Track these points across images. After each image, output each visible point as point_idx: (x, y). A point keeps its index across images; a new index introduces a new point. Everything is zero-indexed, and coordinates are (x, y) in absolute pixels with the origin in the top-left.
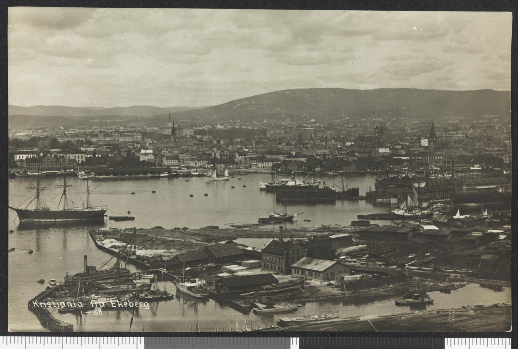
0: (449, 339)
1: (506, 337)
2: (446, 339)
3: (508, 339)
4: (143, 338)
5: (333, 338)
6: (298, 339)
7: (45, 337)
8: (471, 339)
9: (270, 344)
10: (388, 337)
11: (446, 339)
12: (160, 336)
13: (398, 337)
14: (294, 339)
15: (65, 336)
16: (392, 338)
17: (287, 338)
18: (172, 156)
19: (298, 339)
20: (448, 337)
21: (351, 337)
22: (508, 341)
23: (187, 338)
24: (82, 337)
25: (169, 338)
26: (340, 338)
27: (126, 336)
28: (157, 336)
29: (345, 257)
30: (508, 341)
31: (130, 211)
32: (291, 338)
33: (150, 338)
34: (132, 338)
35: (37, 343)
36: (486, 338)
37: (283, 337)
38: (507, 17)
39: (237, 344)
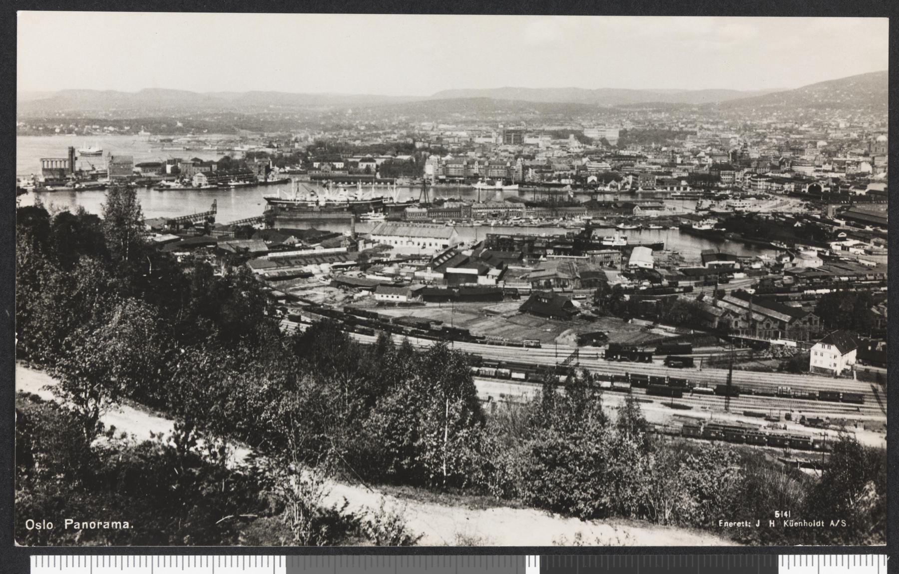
0: (786, 556)
1: (61, 554)
2: (780, 556)
3: (881, 556)
4: (284, 558)
5: (596, 556)
6: (538, 557)
7: (124, 556)
8: (822, 556)
9: (371, 565)
10: (685, 553)
11: (780, 556)
12: (312, 554)
13: (701, 554)
14: (532, 557)
15: (156, 554)
16: (692, 556)
17: (520, 557)
18: (639, 127)
19: (538, 557)
20: (783, 553)
21: (624, 553)
22: (883, 559)
23: (356, 557)
24: (50, 556)
25: (326, 557)
26: (608, 556)
27: (878, 553)
28: (307, 554)
29: (803, 469)
30: (883, 559)
31: (71, 146)
32: (527, 557)
33: (295, 557)
34: (804, 556)
35: (469, 566)
36: (846, 554)
37: (514, 554)
38: (883, 23)
39: (384, 565)
